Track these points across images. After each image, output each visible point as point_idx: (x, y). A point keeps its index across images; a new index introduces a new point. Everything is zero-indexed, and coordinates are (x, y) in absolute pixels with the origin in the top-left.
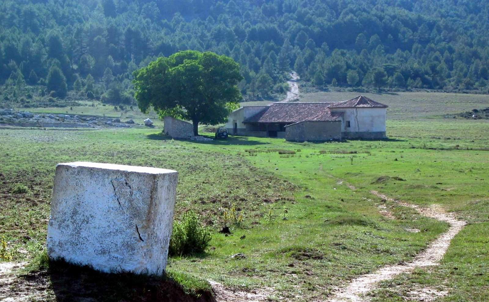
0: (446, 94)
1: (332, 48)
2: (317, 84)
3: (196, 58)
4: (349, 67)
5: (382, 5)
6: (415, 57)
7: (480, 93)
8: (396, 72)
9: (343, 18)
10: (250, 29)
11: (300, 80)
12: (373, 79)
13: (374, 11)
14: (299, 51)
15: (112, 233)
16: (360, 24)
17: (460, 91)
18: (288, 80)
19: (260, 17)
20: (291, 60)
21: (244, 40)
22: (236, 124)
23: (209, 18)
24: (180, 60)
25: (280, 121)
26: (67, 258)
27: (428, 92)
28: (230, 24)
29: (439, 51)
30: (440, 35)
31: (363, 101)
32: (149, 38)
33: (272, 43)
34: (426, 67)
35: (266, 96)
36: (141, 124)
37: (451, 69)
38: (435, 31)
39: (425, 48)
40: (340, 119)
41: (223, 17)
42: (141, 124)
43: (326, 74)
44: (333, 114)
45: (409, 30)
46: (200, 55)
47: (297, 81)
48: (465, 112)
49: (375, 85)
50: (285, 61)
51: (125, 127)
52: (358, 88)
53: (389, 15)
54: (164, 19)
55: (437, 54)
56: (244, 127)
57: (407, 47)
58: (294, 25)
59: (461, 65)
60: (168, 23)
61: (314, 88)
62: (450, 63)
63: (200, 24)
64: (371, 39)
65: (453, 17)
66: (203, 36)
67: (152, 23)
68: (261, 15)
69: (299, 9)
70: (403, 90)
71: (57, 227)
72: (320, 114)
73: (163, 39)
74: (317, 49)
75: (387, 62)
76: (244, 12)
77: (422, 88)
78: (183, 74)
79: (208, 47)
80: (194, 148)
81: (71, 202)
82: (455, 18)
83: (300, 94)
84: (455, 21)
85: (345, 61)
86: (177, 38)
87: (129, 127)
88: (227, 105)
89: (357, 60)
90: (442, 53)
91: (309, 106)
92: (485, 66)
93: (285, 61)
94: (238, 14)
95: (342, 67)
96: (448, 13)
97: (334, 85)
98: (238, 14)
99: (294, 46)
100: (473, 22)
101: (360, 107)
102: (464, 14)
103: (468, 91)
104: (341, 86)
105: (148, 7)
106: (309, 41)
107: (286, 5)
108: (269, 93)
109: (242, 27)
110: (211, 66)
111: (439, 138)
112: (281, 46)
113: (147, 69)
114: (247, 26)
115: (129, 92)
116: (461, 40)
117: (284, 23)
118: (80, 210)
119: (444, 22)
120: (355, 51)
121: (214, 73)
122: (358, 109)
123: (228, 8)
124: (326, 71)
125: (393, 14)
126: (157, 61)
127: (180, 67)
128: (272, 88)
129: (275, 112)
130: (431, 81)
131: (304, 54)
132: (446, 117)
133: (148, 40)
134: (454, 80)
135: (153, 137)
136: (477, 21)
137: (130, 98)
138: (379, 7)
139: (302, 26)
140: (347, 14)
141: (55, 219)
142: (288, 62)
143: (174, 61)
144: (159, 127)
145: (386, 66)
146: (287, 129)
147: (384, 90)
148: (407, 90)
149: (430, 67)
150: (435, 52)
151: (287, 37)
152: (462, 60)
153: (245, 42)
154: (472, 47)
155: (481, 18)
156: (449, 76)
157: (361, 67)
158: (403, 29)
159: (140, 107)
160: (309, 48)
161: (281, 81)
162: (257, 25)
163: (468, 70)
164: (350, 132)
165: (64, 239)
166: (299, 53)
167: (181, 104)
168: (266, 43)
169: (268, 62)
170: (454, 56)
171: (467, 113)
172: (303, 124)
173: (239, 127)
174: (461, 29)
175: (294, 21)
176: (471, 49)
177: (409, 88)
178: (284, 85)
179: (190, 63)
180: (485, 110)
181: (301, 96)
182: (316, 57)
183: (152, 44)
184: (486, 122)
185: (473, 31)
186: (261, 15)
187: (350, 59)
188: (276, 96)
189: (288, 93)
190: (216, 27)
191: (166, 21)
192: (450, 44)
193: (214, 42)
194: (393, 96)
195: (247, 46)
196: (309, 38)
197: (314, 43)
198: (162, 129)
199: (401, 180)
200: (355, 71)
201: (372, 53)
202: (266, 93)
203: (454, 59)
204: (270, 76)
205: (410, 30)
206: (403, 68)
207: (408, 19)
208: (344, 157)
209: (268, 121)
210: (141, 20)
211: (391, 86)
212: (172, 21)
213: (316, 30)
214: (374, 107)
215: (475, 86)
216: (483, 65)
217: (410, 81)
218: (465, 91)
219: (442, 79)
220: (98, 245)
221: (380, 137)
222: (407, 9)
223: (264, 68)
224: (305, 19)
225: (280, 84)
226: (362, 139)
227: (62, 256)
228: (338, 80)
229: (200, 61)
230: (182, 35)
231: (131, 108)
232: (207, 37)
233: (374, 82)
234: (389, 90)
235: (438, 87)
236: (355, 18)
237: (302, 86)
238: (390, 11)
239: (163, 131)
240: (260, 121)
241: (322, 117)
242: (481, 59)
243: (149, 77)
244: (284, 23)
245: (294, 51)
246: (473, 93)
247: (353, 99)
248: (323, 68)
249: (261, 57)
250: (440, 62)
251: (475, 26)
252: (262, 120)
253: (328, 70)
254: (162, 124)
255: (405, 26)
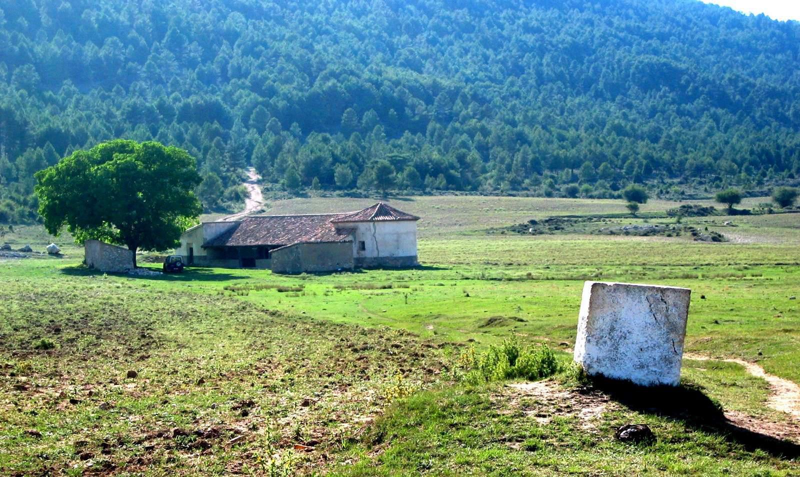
0: (483, 198)
1: (306, 130)
2: (289, 186)
3: (132, 151)
4: (336, 160)
5: (377, 65)
6: (431, 142)
7: (533, 196)
8: (408, 166)
9: (320, 85)
10: (181, 105)
11: (263, 180)
12: (374, 176)
13: (366, 75)
14: (257, 136)
15: (650, 349)
16: (347, 94)
17: (504, 193)
18: (244, 181)
19: (195, 86)
20: (247, 150)
21: (172, 120)
22: (191, 250)
23: (118, 88)
24: (107, 155)
25: (260, 243)
26: (606, 374)
27: (456, 195)
28: (149, 97)
29: (466, 132)
30: (467, 108)
31: (383, 211)
32: (28, 120)
33: (216, 125)
34: (450, 158)
35: (214, 207)
36: (42, 252)
37: (486, 159)
38: (459, 101)
39: (445, 130)
40: (350, 238)
41: (139, 84)
42: (42, 252)
43: (302, 172)
44: (339, 231)
45: (421, 101)
46: (138, 146)
47: (259, 182)
48: (517, 224)
49: (378, 187)
50: (238, 153)
51: (19, 256)
52: (352, 191)
53: (390, 81)
54: (47, 91)
55: (465, 137)
56: (204, 253)
57: (420, 127)
58: (247, 97)
59: (501, 153)
60: (54, 96)
61: (286, 193)
62: (484, 149)
63: (103, 98)
64: (364, 117)
65: (484, 82)
66: (110, 116)
67: (30, 95)
68: (196, 82)
69: (253, 73)
70: (419, 193)
71: (595, 344)
72: (319, 232)
73: (50, 121)
74: (285, 133)
75: (393, 152)
76: (170, 79)
77: (447, 189)
78: (113, 175)
79: (119, 133)
80: (144, 286)
81: (608, 319)
82: (488, 83)
83: (267, 202)
84: (487, 87)
85: (330, 151)
86: (70, 120)
87: (25, 257)
88: (180, 220)
89: (347, 149)
90: (471, 135)
91: (301, 220)
92: (537, 155)
93: (238, 153)
94: (159, 81)
95: (325, 160)
96: (476, 75)
97: (316, 188)
98: (159, 81)
99: (248, 130)
100: (515, 89)
101: (380, 221)
102: (499, 76)
103: (514, 192)
104: (325, 190)
105: (21, 72)
106: (271, 121)
107: (233, 66)
108: (219, 201)
109: (169, 100)
110: (154, 163)
111: (496, 264)
112: (230, 129)
113: (57, 169)
114: (176, 100)
115: (4, 203)
116: (499, 115)
117: (231, 94)
118: (617, 327)
119: (471, 89)
120: (340, 135)
121: (159, 174)
122: (376, 223)
123: (145, 72)
124: (302, 167)
125: (395, 78)
126: (73, 157)
127: (108, 166)
128: (222, 192)
129: (250, 230)
130: (459, 179)
131: (265, 142)
132: (490, 232)
133: (26, 123)
134: (492, 177)
135: (69, 271)
136: (520, 87)
137: (6, 212)
138: (374, 67)
139: (260, 99)
140: (326, 79)
141: (593, 336)
142: (243, 154)
143: (97, 156)
144: (75, 255)
145: (391, 157)
146: (274, 255)
147: (391, 194)
148: (426, 194)
149: (457, 158)
150: (461, 134)
151: (236, 115)
152: (502, 145)
153: (174, 123)
154: (516, 127)
155: (525, 82)
156: (484, 171)
157: (355, 159)
158: (411, 100)
159: (47, 227)
160: (271, 132)
161: (234, 183)
162: (191, 97)
163: (512, 160)
164: (365, 258)
165: (601, 355)
166: (256, 140)
167: (110, 220)
168: (206, 124)
169: (213, 155)
170: (490, 139)
171: (520, 225)
172: (297, 248)
173: (195, 254)
174: (497, 100)
175: (247, 92)
176: (515, 129)
177: (428, 190)
178: (239, 189)
179: (123, 159)
180: (547, 221)
181: (266, 205)
182: (286, 144)
183: (33, 129)
184: (551, 239)
185: (515, 102)
186: (196, 82)
187: (337, 148)
188: (229, 206)
189: (247, 201)
190: (129, 101)
191: (50, 93)
192: (483, 122)
193: (127, 125)
194: (407, 202)
195: (178, 131)
196: (272, 117)
197: (280, 124)
198: (83, 259)
199: (522, 321)
200: (346, 166)
201: (367, 139)
202: (214, 201)
203: (490, 145)
204: (218, 174)
205: (423, 103)
206: (416, 159)
207: (418, 85)
208: (382, 294)
209: (241, 243)
210: (12, 92)
211: (402, 187)
212: (60, 92)
213: (281, 104)
214: (399, 220)
215: (524, 185)
216: (534, 153)
217: (428, 179)
218: (511, 192)
219: (475, 175)
220: (636, 360)
221: (409, 263)
222: (415, 70)
223: (207, 164)
224: (264, 88)
225: (234, 187)
226: (385, 268)
227: (600, 372)
228: (321, 181)
229: (139, 156)
230: (78, 115)
231: (11, 228)
232: (115, 117)
233: (376, 182)
234: (398, 194)
235: (469, 187)
236: (339, 85)
237: (267, 190)
238: (391, 73)
239: (85, 262)
240: (228, 244)
241: (322, 237)
242: (530, 145)
243: (62, 181)
244: (231, 94)
245: (248, 137)
246: (523, 196)
247: (368, 209)
248: (296, 161)
249: (202, 147)
250: (469, 150)
251: (517, 95)
252: (231, 243)
253: (306, 164)
254: (82, 251)
255: (414, 96)
